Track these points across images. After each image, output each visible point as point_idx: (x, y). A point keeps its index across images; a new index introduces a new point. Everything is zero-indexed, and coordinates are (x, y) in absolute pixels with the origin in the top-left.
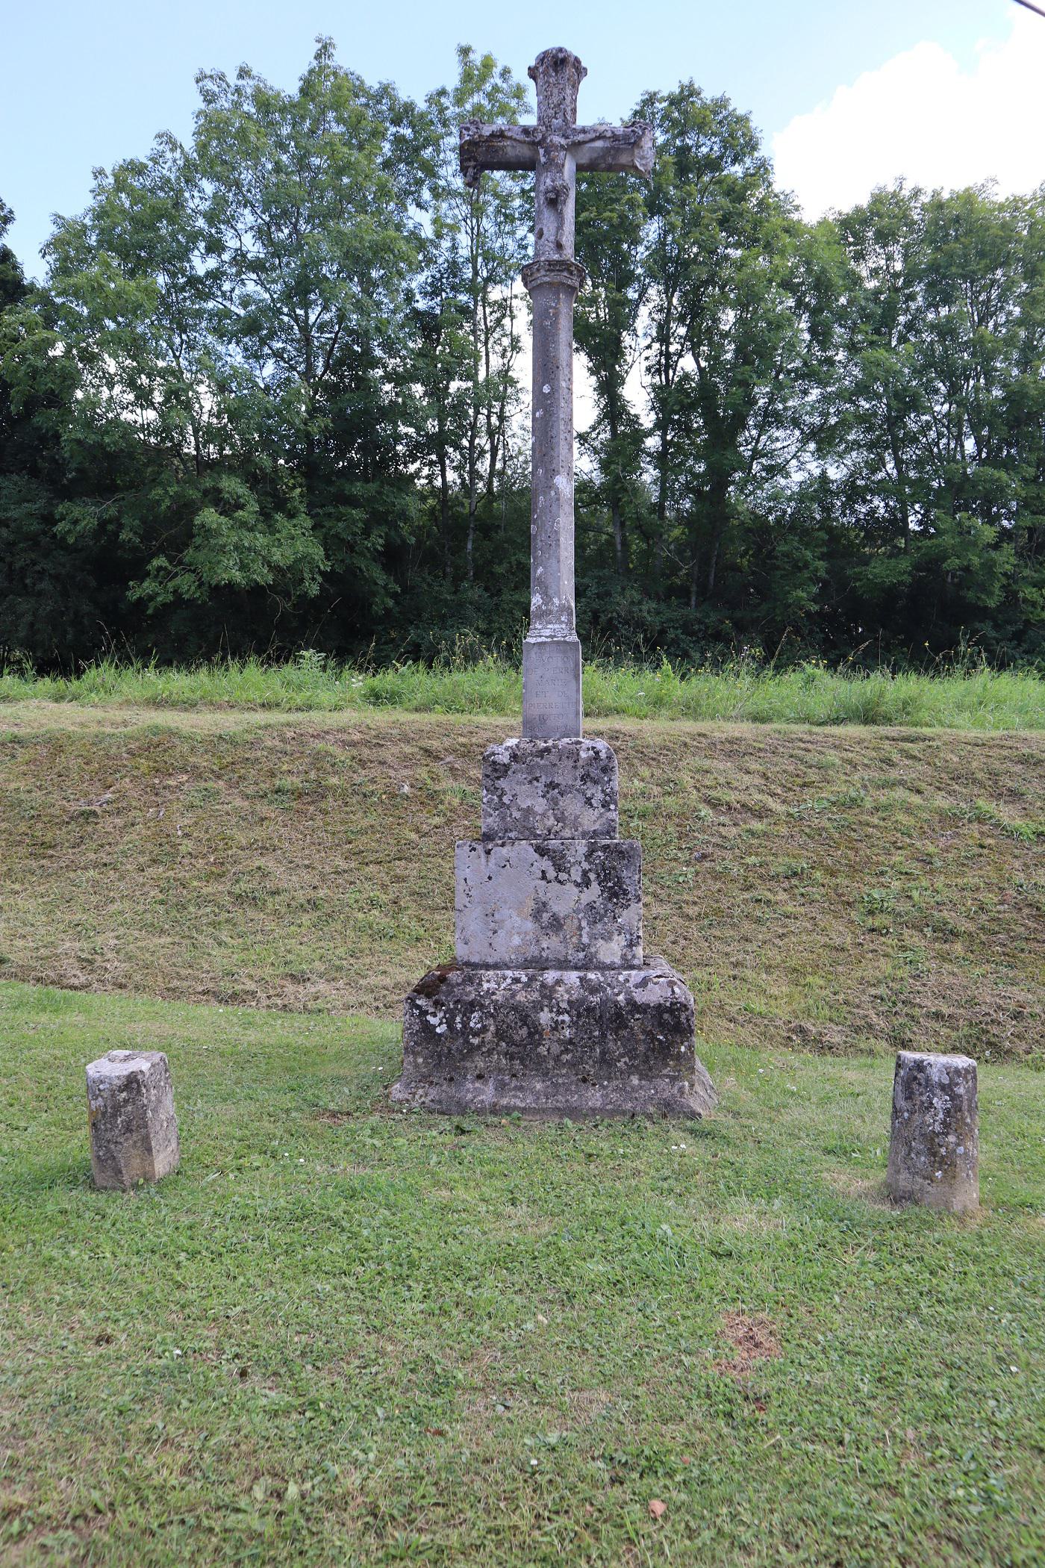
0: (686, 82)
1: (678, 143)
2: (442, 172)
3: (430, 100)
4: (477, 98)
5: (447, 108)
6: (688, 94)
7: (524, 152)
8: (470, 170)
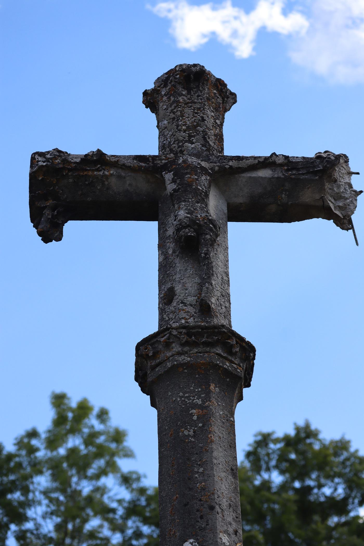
0: (301, 423)
1: (297, 485)
2: (30, 513)
3: (20, 444)
4: (74, 441)
5: (37, 450)
6: (305, 434)
7: (141, 184)
8: (47, 212)
